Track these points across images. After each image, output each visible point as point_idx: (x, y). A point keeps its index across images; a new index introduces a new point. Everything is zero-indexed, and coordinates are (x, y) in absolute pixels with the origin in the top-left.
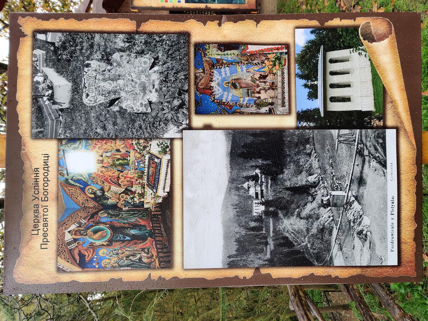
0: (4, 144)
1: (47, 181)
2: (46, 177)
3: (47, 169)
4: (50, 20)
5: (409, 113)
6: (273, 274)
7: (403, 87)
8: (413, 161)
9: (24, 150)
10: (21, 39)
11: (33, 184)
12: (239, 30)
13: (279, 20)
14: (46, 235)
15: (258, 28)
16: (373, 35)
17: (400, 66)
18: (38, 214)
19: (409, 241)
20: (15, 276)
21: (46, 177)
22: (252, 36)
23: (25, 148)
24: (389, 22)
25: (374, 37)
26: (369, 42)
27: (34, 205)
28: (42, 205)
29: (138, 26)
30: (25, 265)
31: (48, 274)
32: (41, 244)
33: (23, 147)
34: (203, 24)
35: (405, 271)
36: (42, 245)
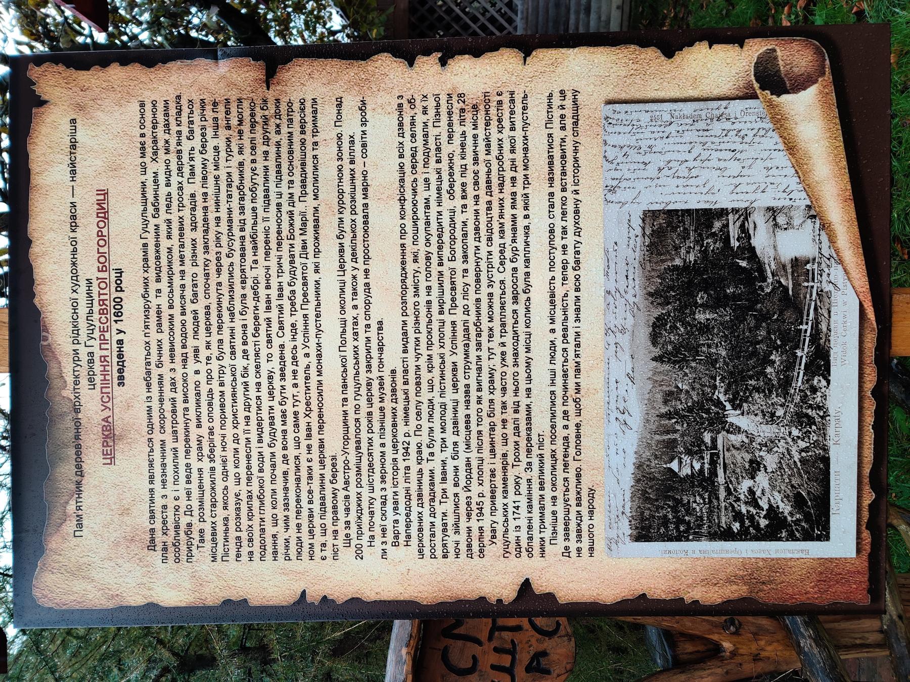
0: (5, 333)
1: (93, 375)
4: (92, 69)
5: (861, 251)
6: (560, 595)
7: (849, 193)
9: (46, 339)
12: (484, 73)
13: (574, 47)
15: (527, 66)
20: (36, 593)
22: (515, 83)
23: (46, 334)
24: (817, 48)
26: (772, 94)
30: (55, 571)
31: (100, 590)
35: (846, 593)
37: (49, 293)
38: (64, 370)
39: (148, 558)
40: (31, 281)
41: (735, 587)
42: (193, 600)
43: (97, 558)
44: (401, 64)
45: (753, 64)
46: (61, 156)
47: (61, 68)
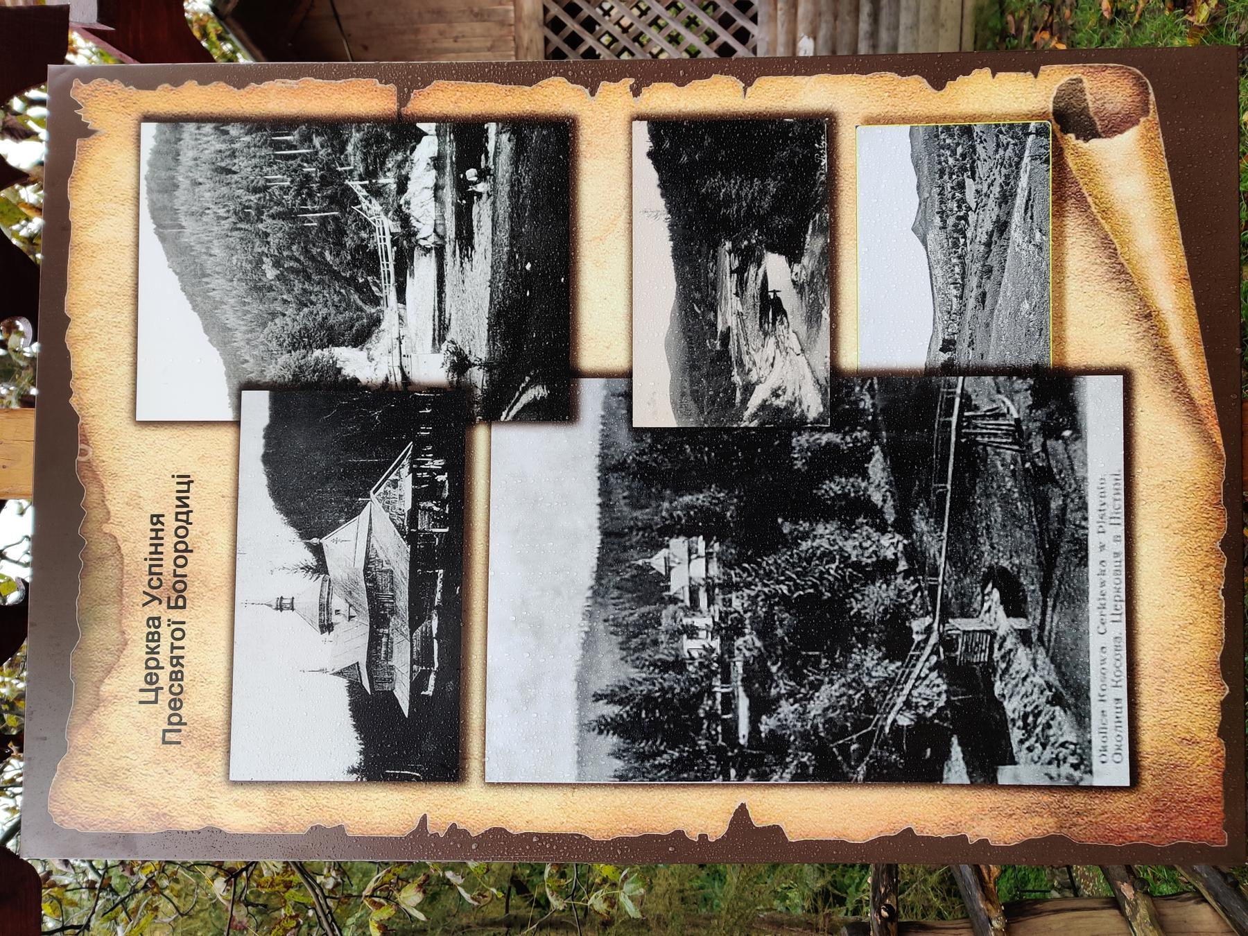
2: (181, 539)
3: (184, 517)
7: (1184, 270)
8: (1216, 494)
9: (84, 453)
10: (79, 142)
11: (146, 559)
14: (178, 704)
16: (1091, 118)
17: (1174, 210)
18: (157, 644)
19: (1204, 735)
21: (181, 539)
24: (1138, 78)
25: (1093, 124)
26: (1077, 138)
27: (149, 619)
28: (169, 620)
29: (403, 100)
30: (82, 777)
31: (141, 805)
32: (165, 731)
33: (81, 446)
34: (587, 91)
35: (1193, 829)
36: (168, 735)
37: (91, 391)
38: (108, 497)
39: (209, 763)
40: (68, 375)
41: (1037, 820)
42: (269, 825)
43: (139, 760)
44: (579, 93)
45: (1052, 99)
46: (114, 206)
47: (117, 85)
